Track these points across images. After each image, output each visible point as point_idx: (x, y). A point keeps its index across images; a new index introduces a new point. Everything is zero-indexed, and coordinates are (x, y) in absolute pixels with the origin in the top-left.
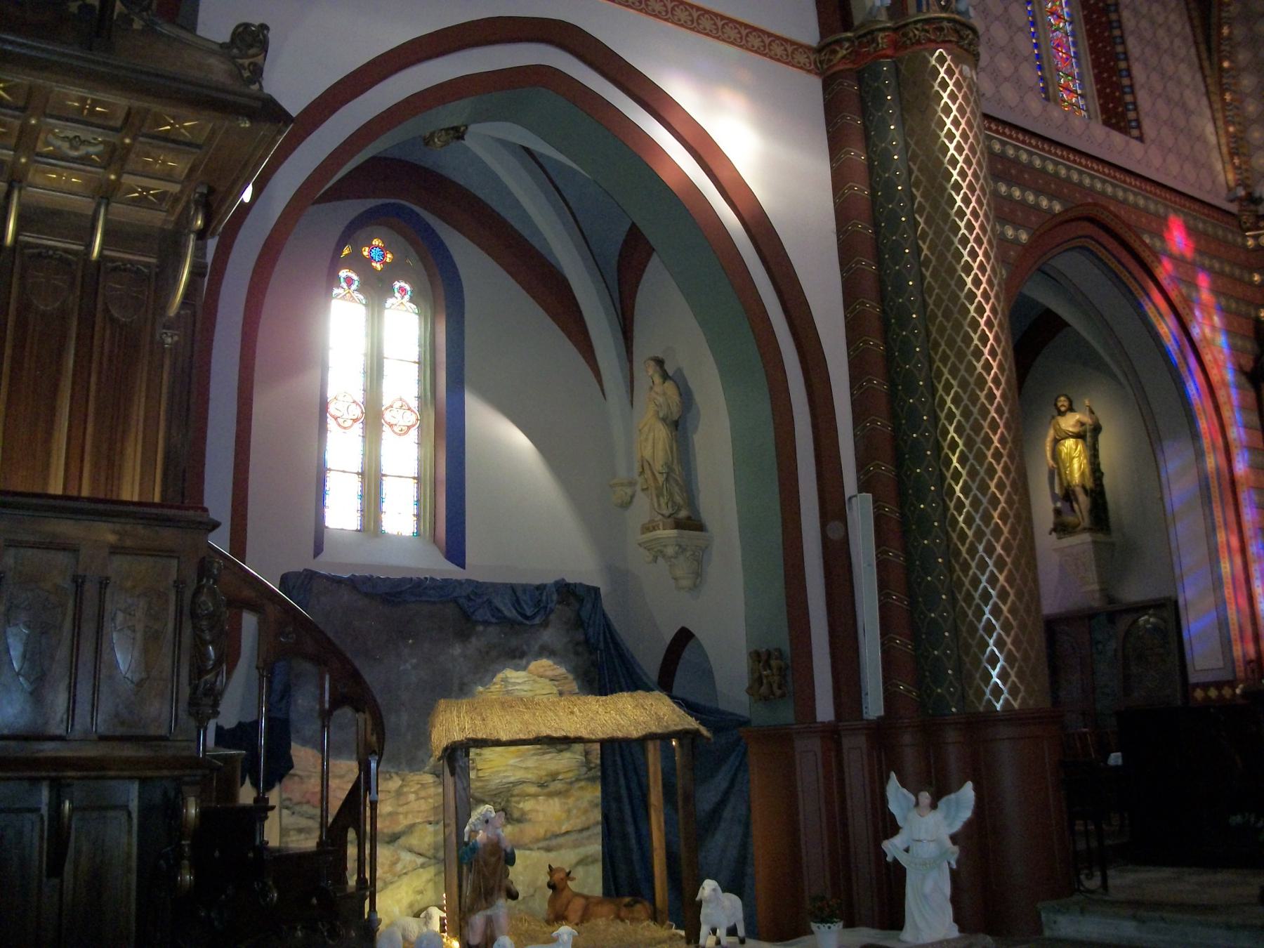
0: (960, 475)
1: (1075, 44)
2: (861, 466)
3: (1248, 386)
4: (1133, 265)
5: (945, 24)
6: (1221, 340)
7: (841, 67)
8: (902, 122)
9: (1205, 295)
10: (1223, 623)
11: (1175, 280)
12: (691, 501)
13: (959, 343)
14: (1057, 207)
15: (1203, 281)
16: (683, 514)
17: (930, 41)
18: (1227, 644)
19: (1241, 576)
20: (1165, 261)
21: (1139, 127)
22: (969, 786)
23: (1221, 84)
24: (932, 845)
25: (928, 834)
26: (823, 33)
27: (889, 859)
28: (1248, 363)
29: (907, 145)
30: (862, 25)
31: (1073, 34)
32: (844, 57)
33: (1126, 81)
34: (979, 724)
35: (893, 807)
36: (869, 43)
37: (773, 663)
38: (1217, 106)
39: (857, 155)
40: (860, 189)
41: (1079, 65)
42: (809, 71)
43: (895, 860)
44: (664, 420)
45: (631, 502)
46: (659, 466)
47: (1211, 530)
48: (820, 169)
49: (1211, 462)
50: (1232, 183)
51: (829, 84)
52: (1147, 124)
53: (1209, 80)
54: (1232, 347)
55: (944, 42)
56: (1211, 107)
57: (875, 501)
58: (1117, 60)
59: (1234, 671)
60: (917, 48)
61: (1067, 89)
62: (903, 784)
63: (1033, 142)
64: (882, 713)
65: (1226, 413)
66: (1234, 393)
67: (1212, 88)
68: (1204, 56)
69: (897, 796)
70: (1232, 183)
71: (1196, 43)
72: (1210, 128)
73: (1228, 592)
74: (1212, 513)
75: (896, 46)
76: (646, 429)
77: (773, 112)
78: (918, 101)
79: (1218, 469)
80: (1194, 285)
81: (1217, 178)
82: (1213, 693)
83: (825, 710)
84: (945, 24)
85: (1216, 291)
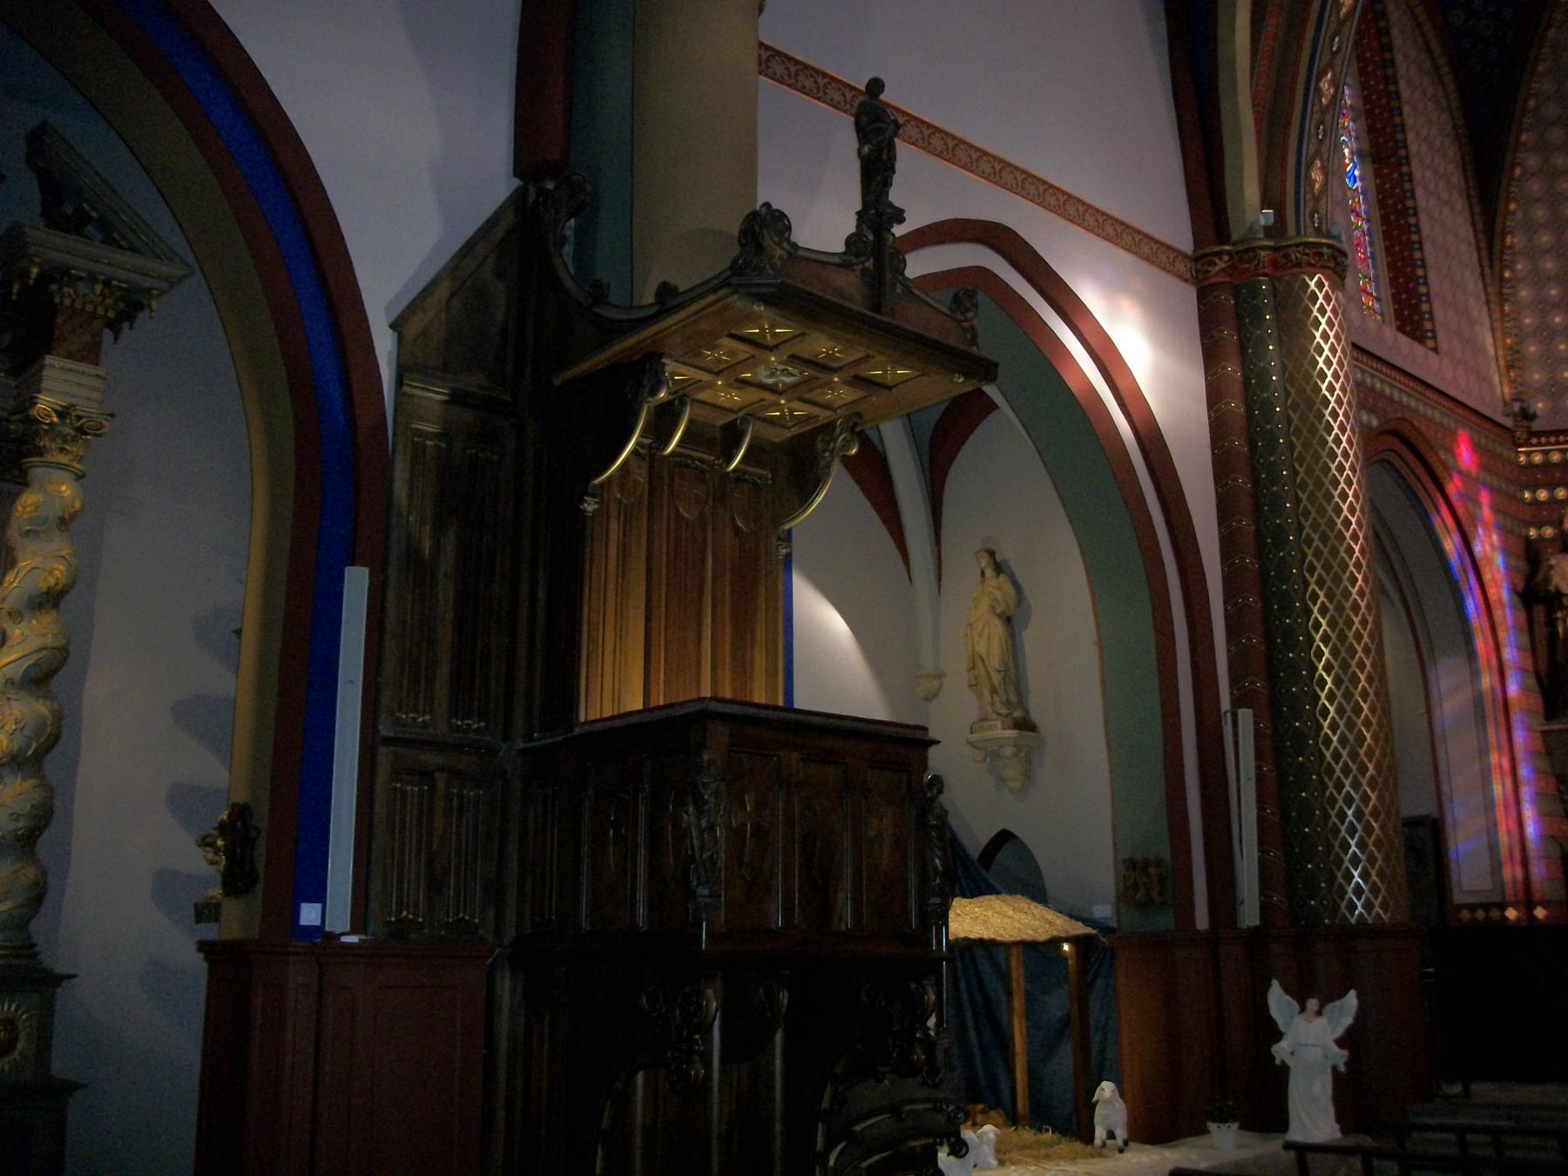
0: (1328, 698)
1: (1371, 244)
2: (1234, 681)
3: (1520, 606)
4: (1426, 478)
5: (1325, 250)
6: (1498, 560)
7: (1219, 280)
8: (1280, 343)
9: (1486, 512)
10: (1493, 846)
11: (1465, 497)
12: (1021, 701)
13: (1336, 568)
14: (1375, 423)
15: (1485, 498)
16: (1018, 714)
17: (1310, 264)
18: (1496, 867)
19: (1511, 799)
20: (1455, 475)
21: (1434, 338)
22: (1352, 994)
23: (1501, 293)
24: (1319, 1050)
25: (1311, 1038)
26: (1198, 243)
27: (1278, 1062)
28: (1521, 585)
29: (1284, 368)
30: (1242, 241)
31: (1370, 234)
32: (1223, 270)
33: (1423, 289)
34: (1350, 935)
35: (1274, 1013)
36: (1249, 262)
37: (1152, 870)
38: (1497, 316)
39: (1232, 370)
40: (1235, 405)
41: (1374, 267)
42: (1186, 280)
43: (1283, 1062)
44: (999, 616)
45: (935, 696)
46: (995, 663)
47: (1484, 751)
48: (1195, 380)
49: (1487, 681)
50: (1507, 397)
51: (1203, 294)
52: (1441, 335)
53: (1490, 289)
54: (1507, 567)
55: (1323, 267)
56: (1490, 316)
57: (1255, 716)
58: (1415, 266)
59: (1503, 892)
60: (1296, 270)
61: (1364, 291)
62: (1287, 990)
63: (1543, 440)
64: (1257, 923)
65: (1502, 635)
66: (1508, 612)
67: (1493, 298)
68: (1486, 262)
69: (1278, 1001)
70: (1507, 397)
71: (1479, 250)
72: (1489, 340)
73: (1500, 813)
74: (1485, 730)
75: (1275, 264)
76: (980, 624)
77: (1160, 318)
78: (1295, 327)
79: (1493, 689)
80: (1478, 503)
81: (1492, 390)
82: (1480, 914)
83: (1202, 921)
84: (1325, 250)
85: (1496, 509)
